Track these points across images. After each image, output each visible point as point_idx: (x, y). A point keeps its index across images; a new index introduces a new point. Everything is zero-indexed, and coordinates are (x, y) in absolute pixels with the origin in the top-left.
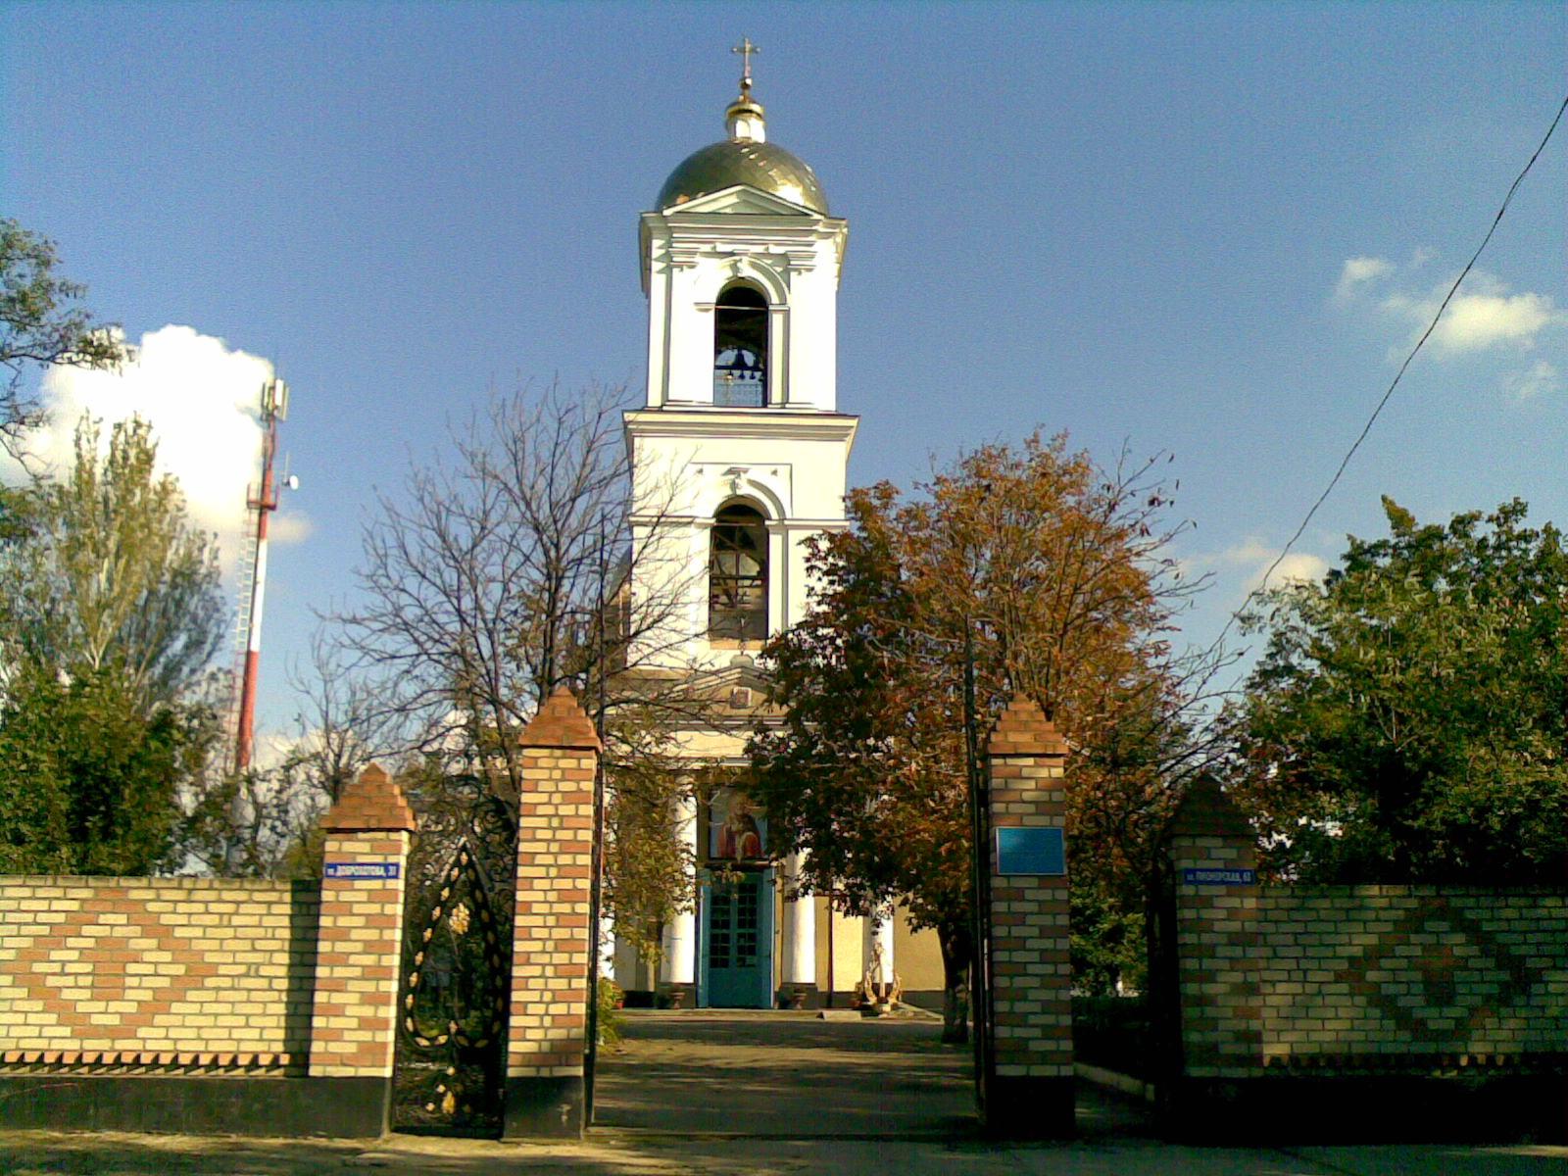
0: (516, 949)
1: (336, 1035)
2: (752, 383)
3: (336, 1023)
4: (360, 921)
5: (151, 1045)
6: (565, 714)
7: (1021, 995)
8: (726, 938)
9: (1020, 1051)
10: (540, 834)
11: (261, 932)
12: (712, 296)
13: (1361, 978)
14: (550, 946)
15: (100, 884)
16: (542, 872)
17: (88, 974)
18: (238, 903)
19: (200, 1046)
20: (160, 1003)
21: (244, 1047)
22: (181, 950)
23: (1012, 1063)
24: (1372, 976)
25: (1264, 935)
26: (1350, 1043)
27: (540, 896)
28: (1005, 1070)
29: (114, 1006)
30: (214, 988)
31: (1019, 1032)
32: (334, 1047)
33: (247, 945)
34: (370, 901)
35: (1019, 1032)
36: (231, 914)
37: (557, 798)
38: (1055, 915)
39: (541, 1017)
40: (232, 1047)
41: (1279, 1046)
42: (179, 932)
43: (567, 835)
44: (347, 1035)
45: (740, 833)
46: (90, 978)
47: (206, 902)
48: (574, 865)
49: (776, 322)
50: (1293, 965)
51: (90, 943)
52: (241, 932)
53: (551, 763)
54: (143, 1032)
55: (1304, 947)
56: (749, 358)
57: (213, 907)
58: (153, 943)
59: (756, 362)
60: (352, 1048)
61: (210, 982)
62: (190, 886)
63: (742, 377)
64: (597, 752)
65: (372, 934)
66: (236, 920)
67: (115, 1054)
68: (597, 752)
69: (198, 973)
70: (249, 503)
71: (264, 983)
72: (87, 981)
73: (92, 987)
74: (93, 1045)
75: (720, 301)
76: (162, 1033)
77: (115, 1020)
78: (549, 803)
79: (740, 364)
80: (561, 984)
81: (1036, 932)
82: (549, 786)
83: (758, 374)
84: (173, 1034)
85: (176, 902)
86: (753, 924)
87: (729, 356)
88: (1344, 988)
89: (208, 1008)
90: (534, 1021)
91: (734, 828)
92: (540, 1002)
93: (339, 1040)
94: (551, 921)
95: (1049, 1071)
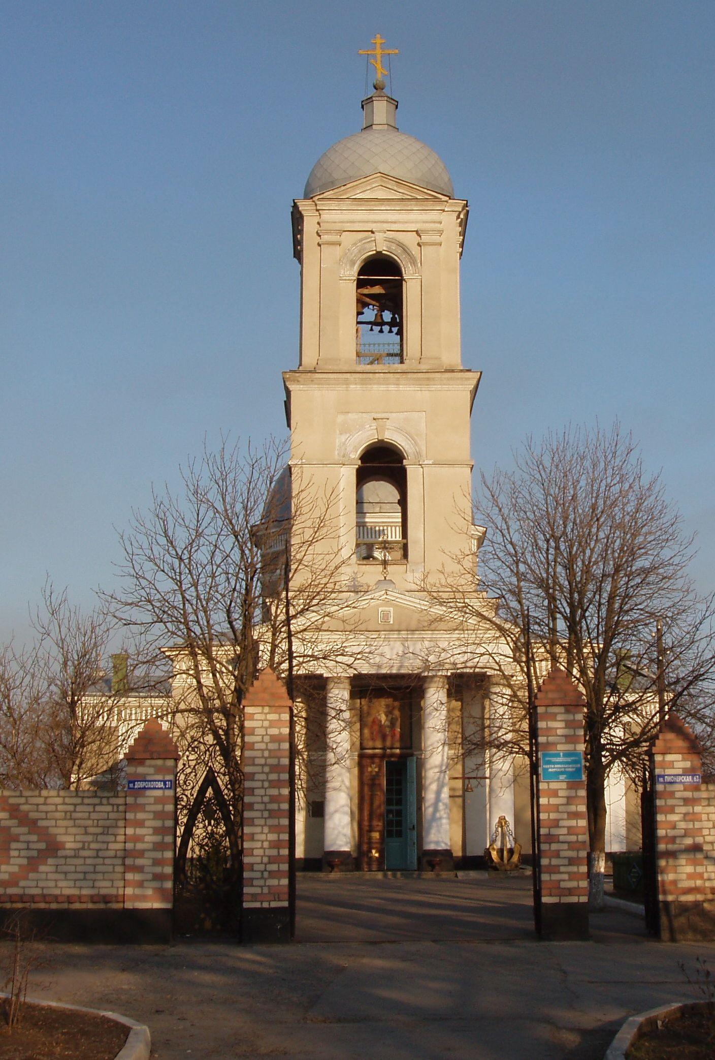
0: (287, 835)
2: (390, 338)
11: (90, 822)
28: (545, 900)
36: (71, 812)
39: (262, 872)
53: (262, 717)
59: (393, 319)
63: (381, 331)
78: (262, 742)
83: (395, 330)
84: (41, 884)
86: (399, 802)
92: (262, 863)
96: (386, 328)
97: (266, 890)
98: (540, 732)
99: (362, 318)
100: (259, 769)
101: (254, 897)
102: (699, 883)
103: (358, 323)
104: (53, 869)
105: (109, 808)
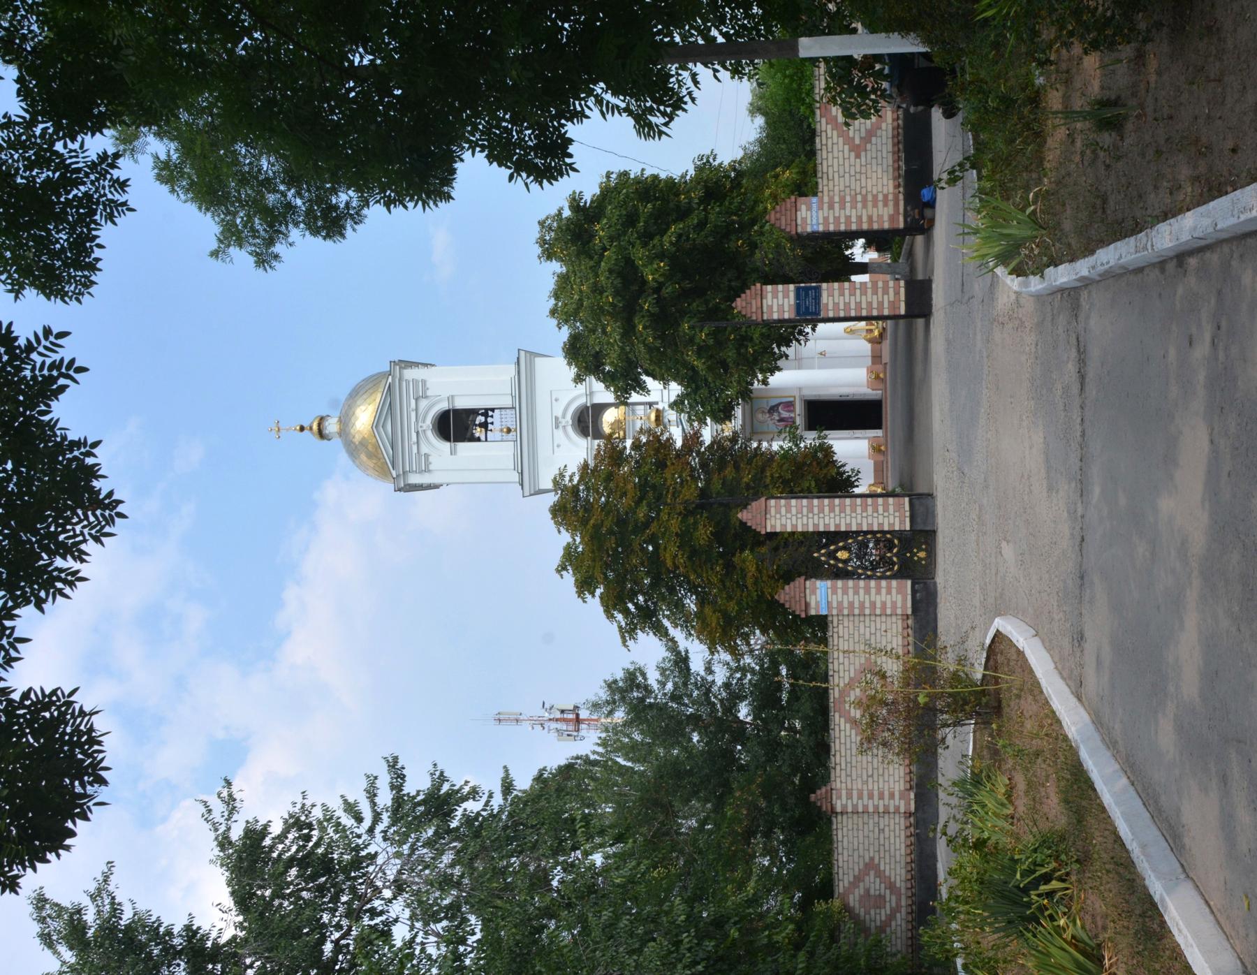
7: (856, 592)
9: (893, 305)
10: (805, 522)
12: (445, 446)
13: (858, 146)
14: (854, 515)
24: (857, 141)
27: (832, 520)
28: (903, 312)
31: (886, 305)
32: (899, 604)
35: (886, 305)
42: (852, 675)
44: (894, 599)
50: (853, 178)
53: (773, 519)
56: (480, 419)
57: (841, 661)
59: (482, 414)
60: (899, 597)
61: (853, 154)
63: (492, 423)
71: (873, 637)
80: (870, 509)
83: (490, 413)
84: (897, 779)
87: (478, 432)
88: (863, 154)
90: (886, 520)
91: (777, 418)
93: (896, 602)
94: (843, 515)
95: (902, 291)
96: (490, 420)
97: (897, 514)
98: (781, 318)
99: (483, 438)
100: (810, 520)
101: (902, 522)
102: (891, 197)
103: (486, 440)
104: (880, 167)
105: (841, 626)
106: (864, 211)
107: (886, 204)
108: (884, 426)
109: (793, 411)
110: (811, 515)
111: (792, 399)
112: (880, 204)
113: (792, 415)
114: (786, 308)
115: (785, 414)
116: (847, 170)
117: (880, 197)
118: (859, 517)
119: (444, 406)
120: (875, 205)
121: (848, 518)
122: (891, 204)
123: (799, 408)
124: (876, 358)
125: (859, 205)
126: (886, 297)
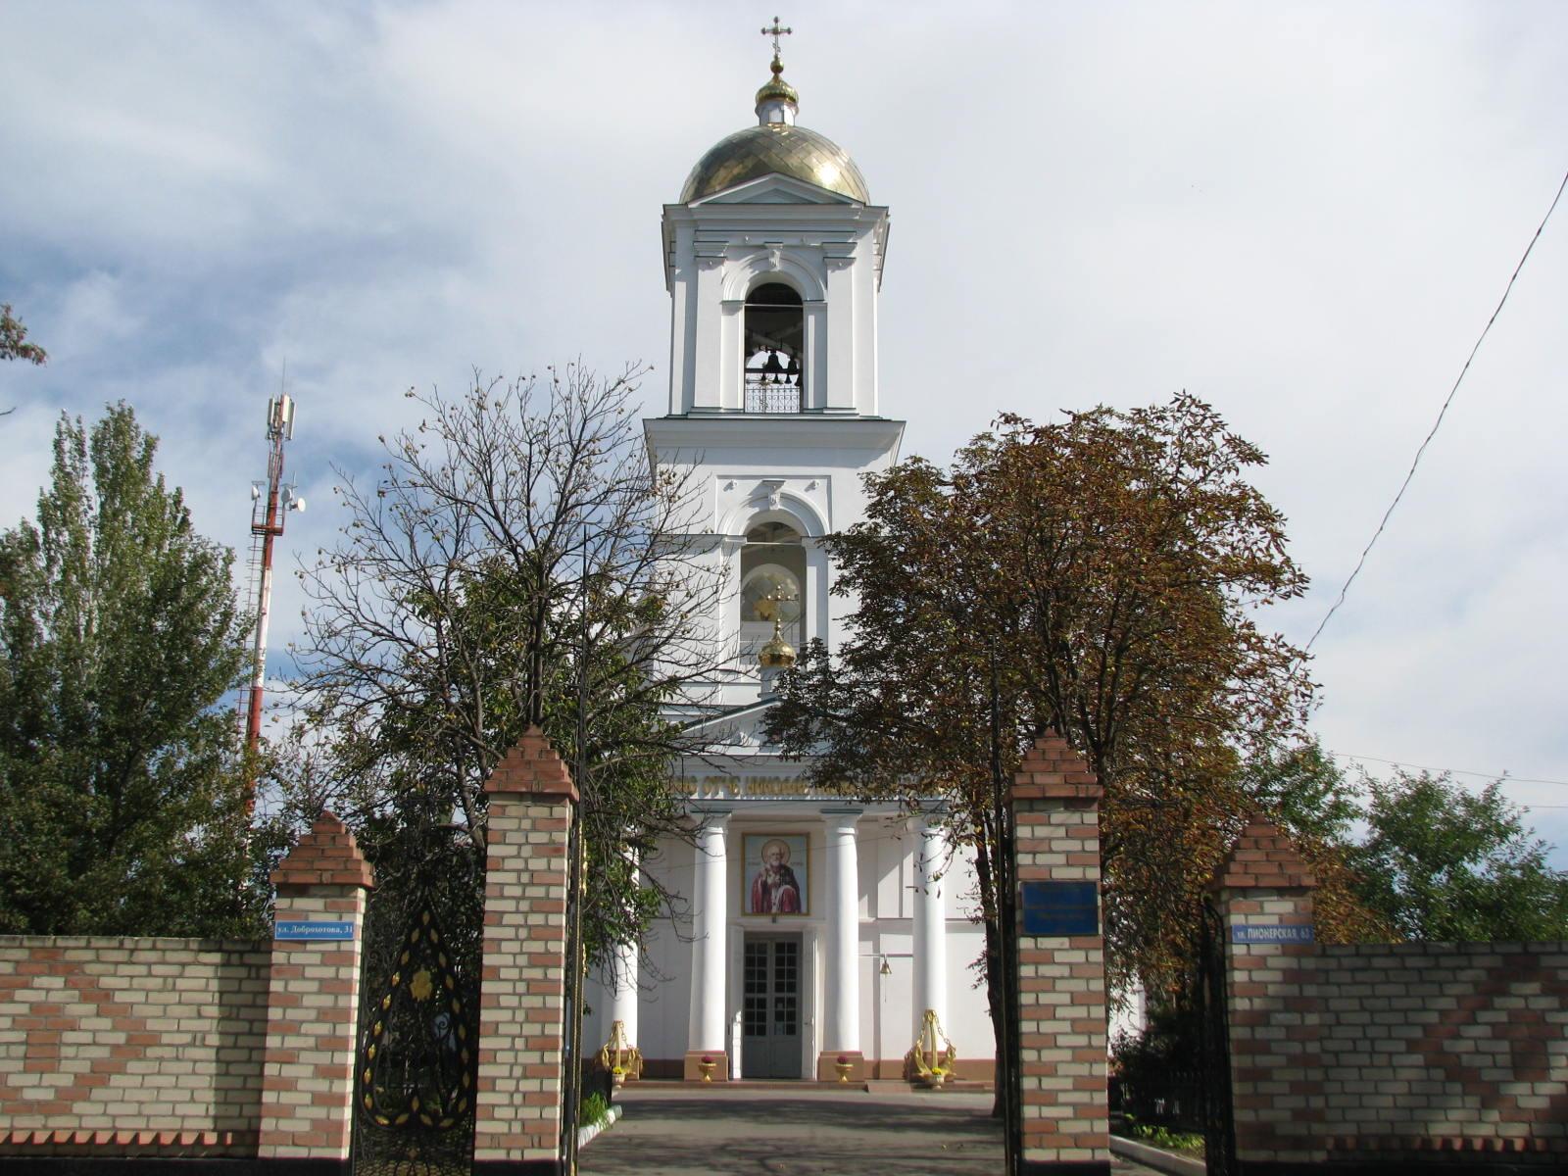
1: (287, 1112)
3: (287, 1098)
4: (314, 986)
5: (88, 1123)
6: (536, 757)
7: (1051, 1070)
8: (762, 1003)
9: (1048, 1131)
10: (508, 891)
14: (520, 1016)
15: (37, 944)
16: (510, 933)
17: (21, 1043)
18: (183, 965)
19: (141, 1123)
20: (98, 1076)
21: (189, 1124)
22: (122, 1016)
23: (1040, 1146)
25: (1326, 999)
26: (1392, 1123)
27: (509, 960)
28: (1032, 1155)
29: (48, 1079)
30: (157, 1059)
31: (1049, 1112)
32: (286, 1125)
33: (192, 1011)
34: (323, 964)
35: (1049, 1112)
36: (175, 977)
37: (526, 851)
38: (1088, 980)
40: (176, 1124)
41: (1448, 1125)
42: (119, 997)
43: (537, 892)
44: (299, 1112)
45: (777, 886)
46: (24, 1047)
47: (149, 964)
48: (546, 926)
49: (811, 322)
51: (24, 1009)
52: (186, 997)
54: (79, 1107)
55: (1372, 1012)
56: (784, 360)
57: (157, 969)
58: (92, 1008)
59: (792, 364)
60: (304, 1127)
61: (151, 1052)
62: (132, 946)
64: (572, 800)
65: (327, 1001)
66: (181, 984)
67: (49, 1133)
68: (572, 800)
69: (139, 1042)
70: (255, 529)
72: (21, 1050)
73: (26, 1057)
74: (25, 1122)
75: (750, 298)
76: (99, 1108)
77: (49, 1095)
78: (518, 856)
79: (773, 366)
81: (1066, 999)
82: (518, 838)
83: (794, 378)
85: (117, 963)
86: (792, 987)
87: (761, 358)
89: (150, 1081)
90: (504, 1099)
91: (770, 881)
94: (521, 987)
95: (1082, 1155)
97: (517, 1128)
101: (495, 1140)
106: (1281, 1060)
107: (1299, 1115)
108: (746, 1082)
109: (782, 911)
110: (524, 906)
111: (804, 909)
112: (1298, 1102)
113: (774, 909)
114: (1041, 859)
115: (776, 895)
116: (1378, 1018)
117: (1317, 1102)
118: (515, 1029)
119: (807, 295)
120: (1296, 1088)
121: (514, 1001)
122: (1301, 1130)
123: (787, 923)
124: (877, 1069)
125: (1295, 1048)
126: (1068, 1112)
